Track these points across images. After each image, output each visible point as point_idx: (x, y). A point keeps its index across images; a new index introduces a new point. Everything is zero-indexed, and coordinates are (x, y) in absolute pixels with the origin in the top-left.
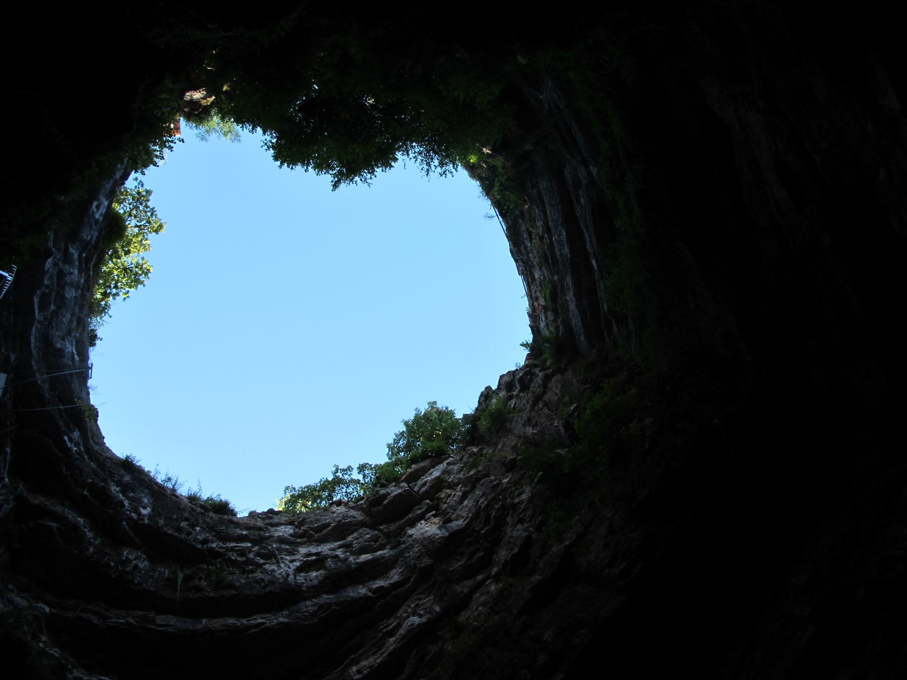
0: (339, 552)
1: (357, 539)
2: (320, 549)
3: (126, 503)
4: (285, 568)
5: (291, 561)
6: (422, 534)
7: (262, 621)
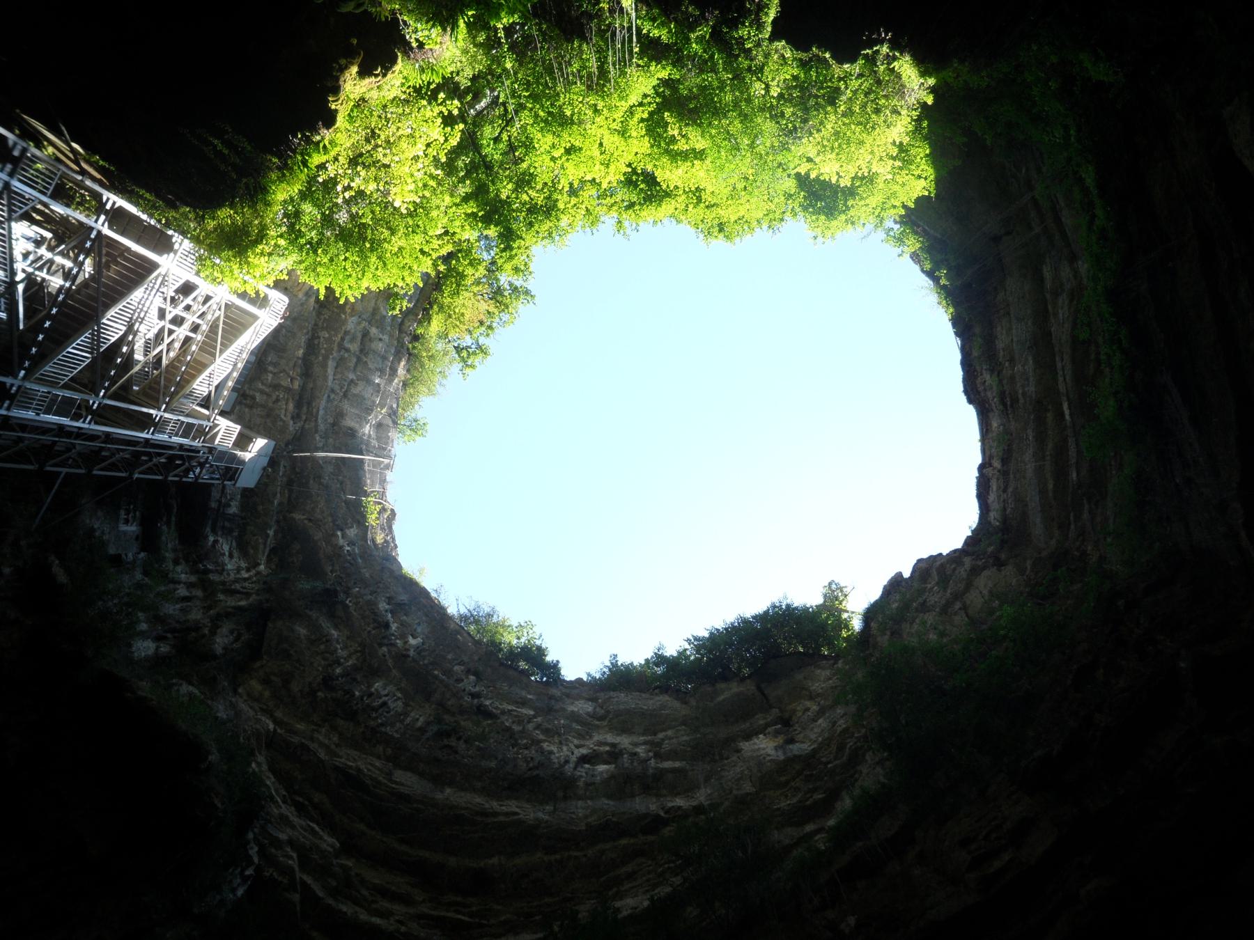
0: (640, 750)
1: (670, 738)
2: (617, 740)
3: (394, 627)
4: (566, 752)
5: (578, 747)
6: (753, 751)
7: (518, 810)
